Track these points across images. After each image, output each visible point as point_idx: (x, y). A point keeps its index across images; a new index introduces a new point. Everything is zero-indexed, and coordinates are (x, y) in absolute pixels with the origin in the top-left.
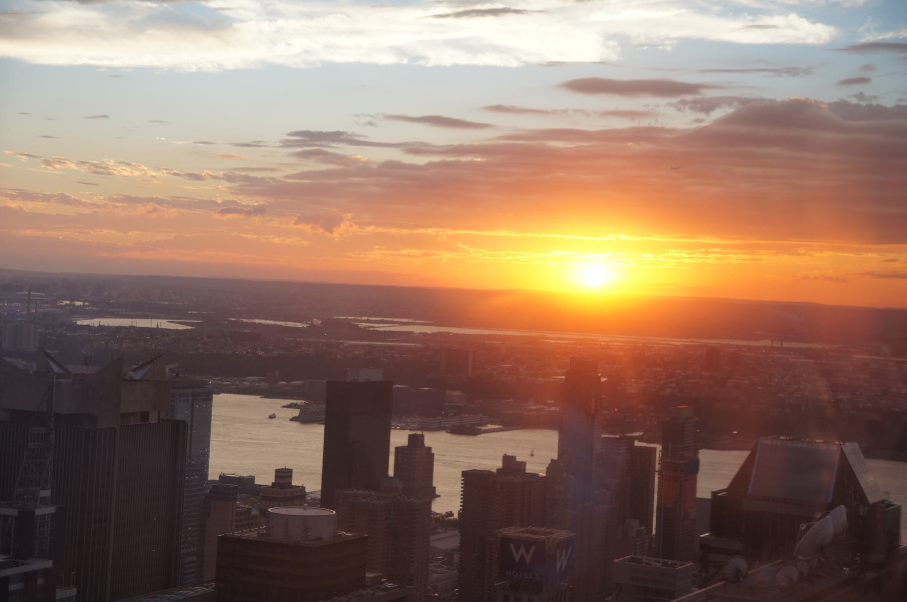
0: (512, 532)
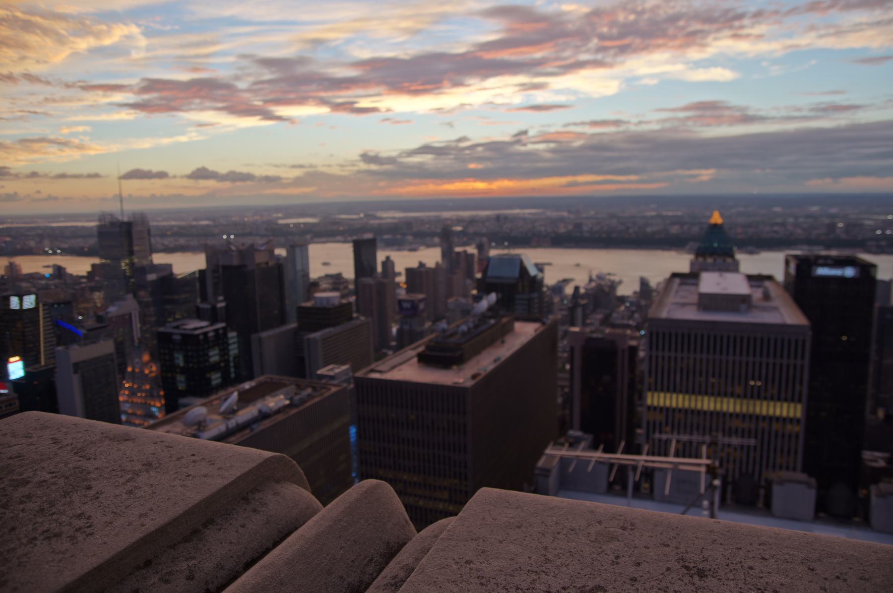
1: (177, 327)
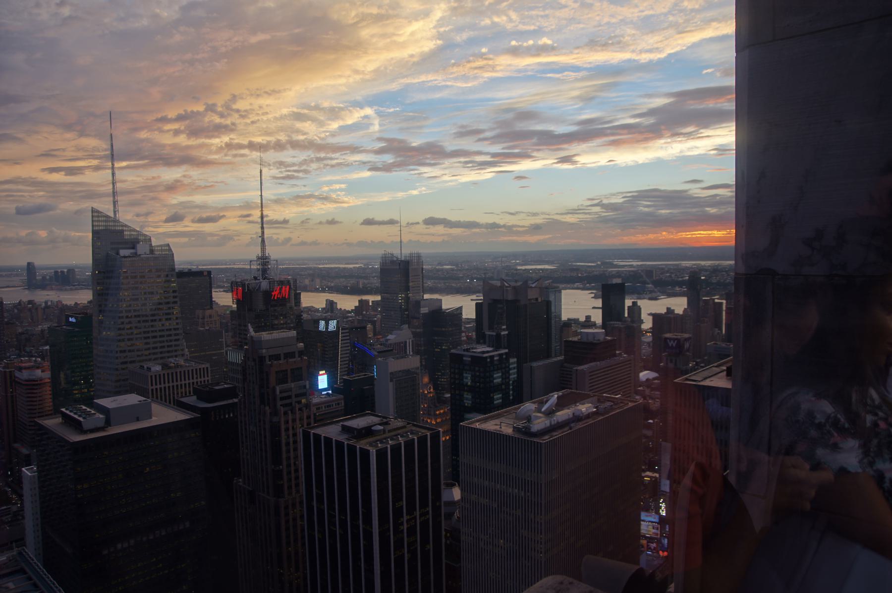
0: (668, 335)
1: (467, 350)
